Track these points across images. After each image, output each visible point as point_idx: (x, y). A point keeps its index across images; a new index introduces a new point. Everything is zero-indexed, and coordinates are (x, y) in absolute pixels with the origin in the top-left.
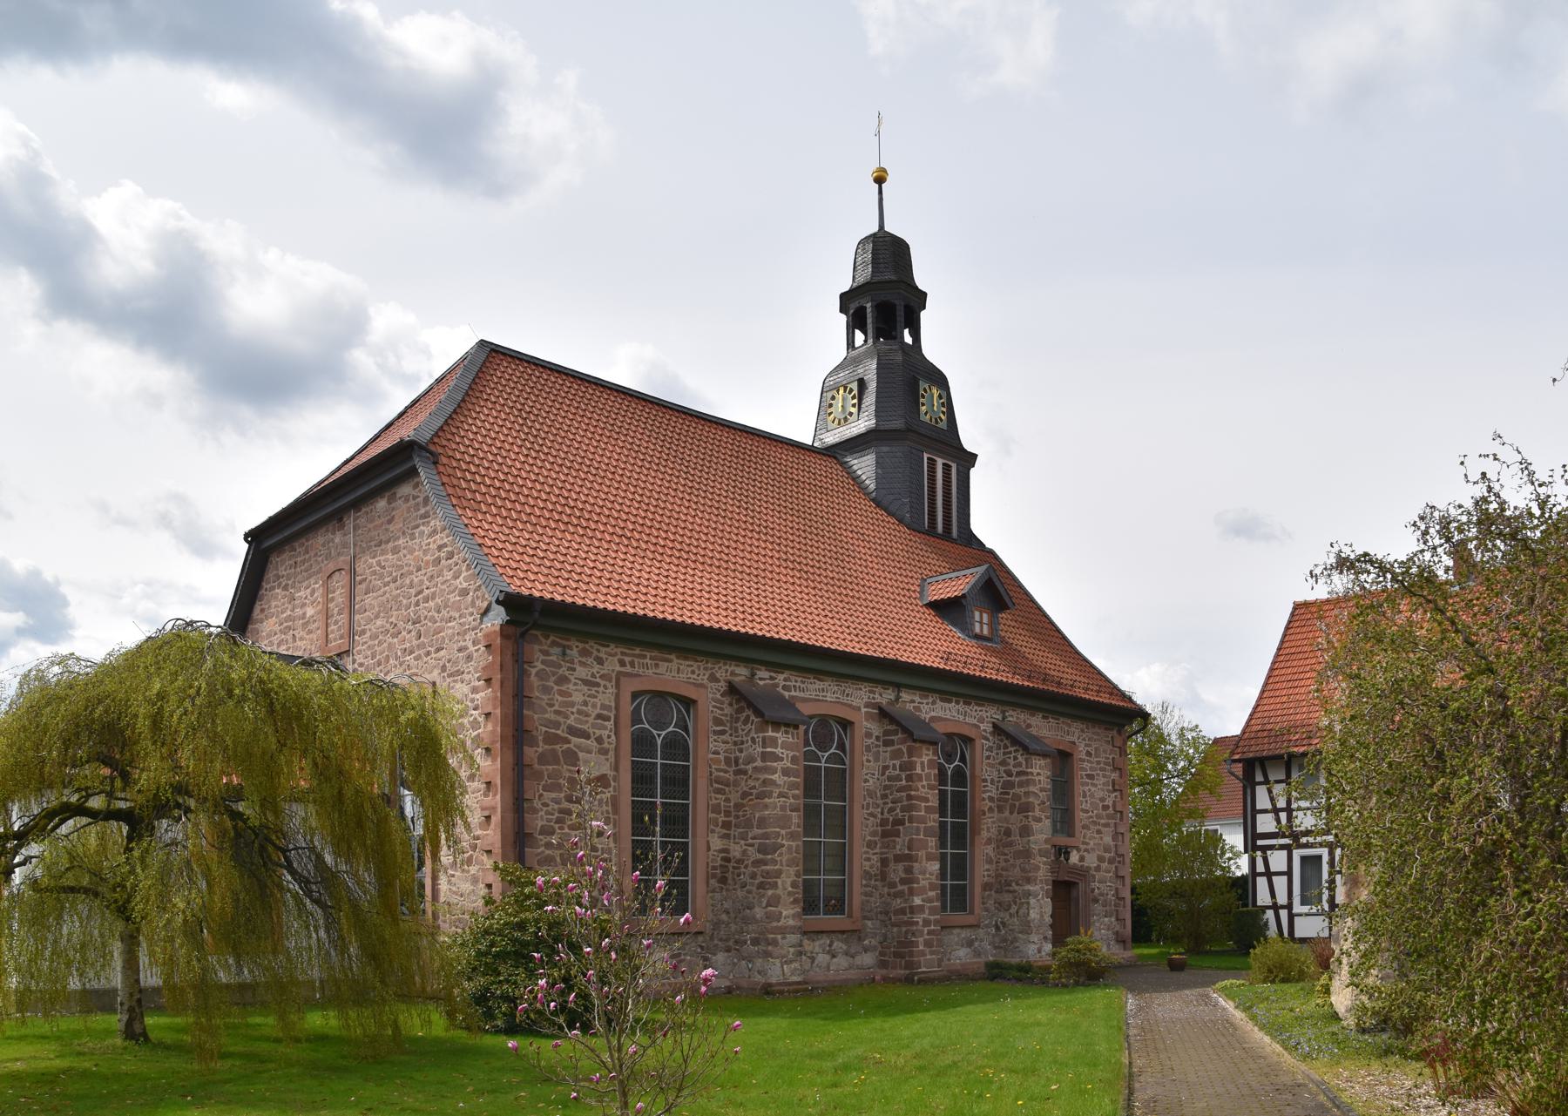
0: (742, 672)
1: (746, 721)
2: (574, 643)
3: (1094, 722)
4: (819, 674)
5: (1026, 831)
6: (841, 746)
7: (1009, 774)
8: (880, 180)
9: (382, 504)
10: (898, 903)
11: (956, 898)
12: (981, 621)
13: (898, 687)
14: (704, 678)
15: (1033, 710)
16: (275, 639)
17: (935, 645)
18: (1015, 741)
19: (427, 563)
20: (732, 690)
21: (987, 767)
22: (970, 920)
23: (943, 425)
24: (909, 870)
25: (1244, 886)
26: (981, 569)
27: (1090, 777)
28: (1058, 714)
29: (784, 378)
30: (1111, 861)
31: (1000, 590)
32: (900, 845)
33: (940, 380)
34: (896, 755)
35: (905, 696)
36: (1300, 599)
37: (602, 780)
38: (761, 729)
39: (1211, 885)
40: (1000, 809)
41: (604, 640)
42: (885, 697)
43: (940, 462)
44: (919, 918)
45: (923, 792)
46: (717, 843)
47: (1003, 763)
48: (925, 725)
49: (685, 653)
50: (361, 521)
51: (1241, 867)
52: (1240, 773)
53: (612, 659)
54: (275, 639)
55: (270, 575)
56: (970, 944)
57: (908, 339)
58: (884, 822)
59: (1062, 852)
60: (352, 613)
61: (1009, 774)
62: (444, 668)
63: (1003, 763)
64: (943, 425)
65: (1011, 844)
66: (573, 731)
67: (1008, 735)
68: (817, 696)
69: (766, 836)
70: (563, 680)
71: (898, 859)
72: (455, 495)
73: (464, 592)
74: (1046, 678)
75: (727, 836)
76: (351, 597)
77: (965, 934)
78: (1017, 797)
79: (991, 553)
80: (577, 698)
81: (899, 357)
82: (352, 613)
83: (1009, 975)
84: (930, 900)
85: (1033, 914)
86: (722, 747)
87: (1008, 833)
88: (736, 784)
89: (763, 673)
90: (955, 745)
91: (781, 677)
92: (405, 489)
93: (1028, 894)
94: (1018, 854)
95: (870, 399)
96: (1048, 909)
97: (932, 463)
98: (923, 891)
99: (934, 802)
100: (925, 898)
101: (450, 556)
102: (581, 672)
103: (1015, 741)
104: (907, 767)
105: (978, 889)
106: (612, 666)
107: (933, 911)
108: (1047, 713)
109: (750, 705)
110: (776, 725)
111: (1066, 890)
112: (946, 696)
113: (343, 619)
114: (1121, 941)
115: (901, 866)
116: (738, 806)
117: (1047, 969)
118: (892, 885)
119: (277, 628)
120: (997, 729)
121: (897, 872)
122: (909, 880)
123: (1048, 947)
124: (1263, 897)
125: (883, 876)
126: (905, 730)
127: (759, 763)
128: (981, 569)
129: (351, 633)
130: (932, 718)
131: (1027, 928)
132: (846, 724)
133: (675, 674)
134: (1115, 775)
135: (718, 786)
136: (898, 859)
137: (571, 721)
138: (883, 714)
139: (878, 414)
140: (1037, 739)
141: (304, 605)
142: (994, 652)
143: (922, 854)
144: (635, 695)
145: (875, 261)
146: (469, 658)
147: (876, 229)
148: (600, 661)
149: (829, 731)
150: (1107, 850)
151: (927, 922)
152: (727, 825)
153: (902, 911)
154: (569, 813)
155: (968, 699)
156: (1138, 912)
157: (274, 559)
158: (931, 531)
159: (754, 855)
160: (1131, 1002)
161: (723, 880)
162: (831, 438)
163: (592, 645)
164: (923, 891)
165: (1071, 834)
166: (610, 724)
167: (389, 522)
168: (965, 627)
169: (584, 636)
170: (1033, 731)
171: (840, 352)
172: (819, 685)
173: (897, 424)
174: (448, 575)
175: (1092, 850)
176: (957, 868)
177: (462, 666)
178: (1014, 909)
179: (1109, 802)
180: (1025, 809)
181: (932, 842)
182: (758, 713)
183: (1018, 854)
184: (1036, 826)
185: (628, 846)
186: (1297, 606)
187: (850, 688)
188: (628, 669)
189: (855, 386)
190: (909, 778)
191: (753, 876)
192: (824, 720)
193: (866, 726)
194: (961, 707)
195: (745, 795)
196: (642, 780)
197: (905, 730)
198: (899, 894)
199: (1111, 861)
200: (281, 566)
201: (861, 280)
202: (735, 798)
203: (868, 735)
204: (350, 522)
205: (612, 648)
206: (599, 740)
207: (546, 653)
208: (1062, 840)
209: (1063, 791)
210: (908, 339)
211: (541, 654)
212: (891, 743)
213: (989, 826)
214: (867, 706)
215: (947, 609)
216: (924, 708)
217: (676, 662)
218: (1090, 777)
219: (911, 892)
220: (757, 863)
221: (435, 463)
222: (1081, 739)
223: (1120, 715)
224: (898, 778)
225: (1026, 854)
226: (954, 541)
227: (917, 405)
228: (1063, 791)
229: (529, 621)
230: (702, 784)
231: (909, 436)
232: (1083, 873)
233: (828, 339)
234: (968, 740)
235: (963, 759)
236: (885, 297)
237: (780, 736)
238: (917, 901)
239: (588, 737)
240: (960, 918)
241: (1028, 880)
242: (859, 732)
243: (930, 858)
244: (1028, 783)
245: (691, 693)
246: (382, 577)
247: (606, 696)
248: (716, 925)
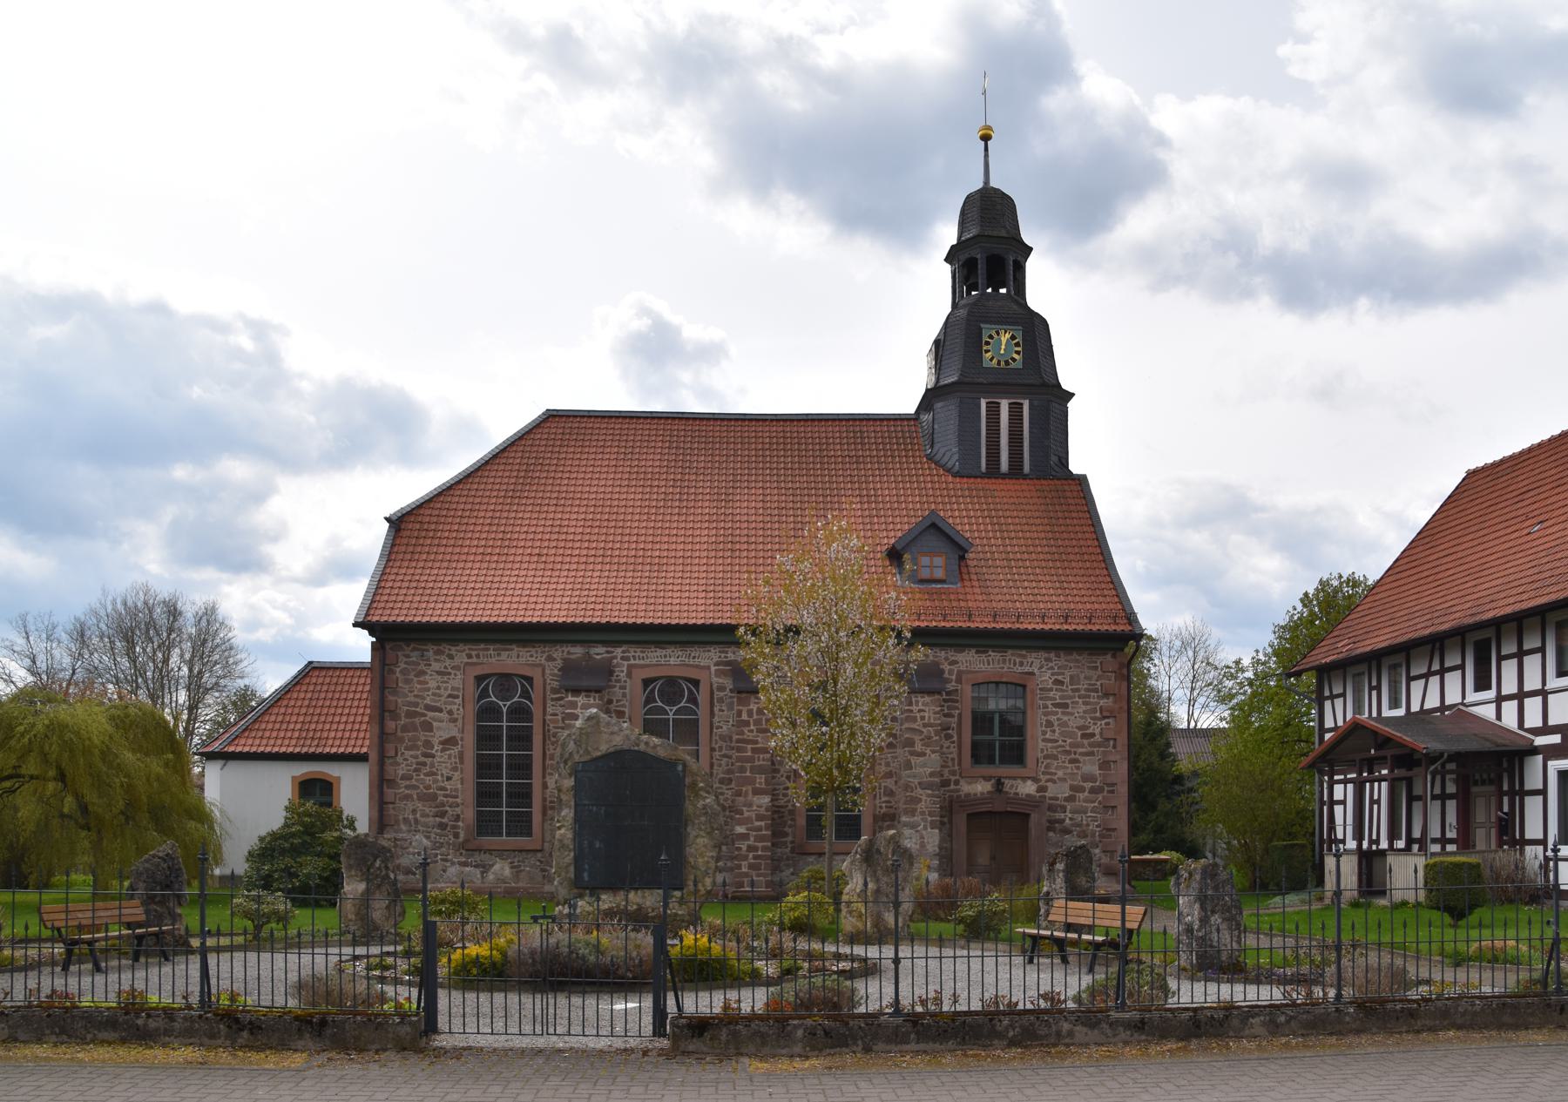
8: (986, 138)
37: (451, 741)
41: (454, 642)
43: (1004, 406)
49: (523, 643)
53: (461, 654)
66: (429, 708)
70: (423, 673)
80: (432, 684)
84: (760, 829)
91: (619, 650)
97: (994, 410)
102: (436, 666)
133: (514, 659)
137: (428, 701)
147: (980, 185)
148: (451, 657)
154: (424, 764)
158: (993, 471)
163: (445, 647)
172: (660, 652)
188: (474, 660)
196: (487, 738)
205: (461, 647)
206: (450, 712)
207: (408, 656)
211: (406, 658)
214: (717, 664)
217: (516, 649)
233: (927, 294)
239: (441, 711)
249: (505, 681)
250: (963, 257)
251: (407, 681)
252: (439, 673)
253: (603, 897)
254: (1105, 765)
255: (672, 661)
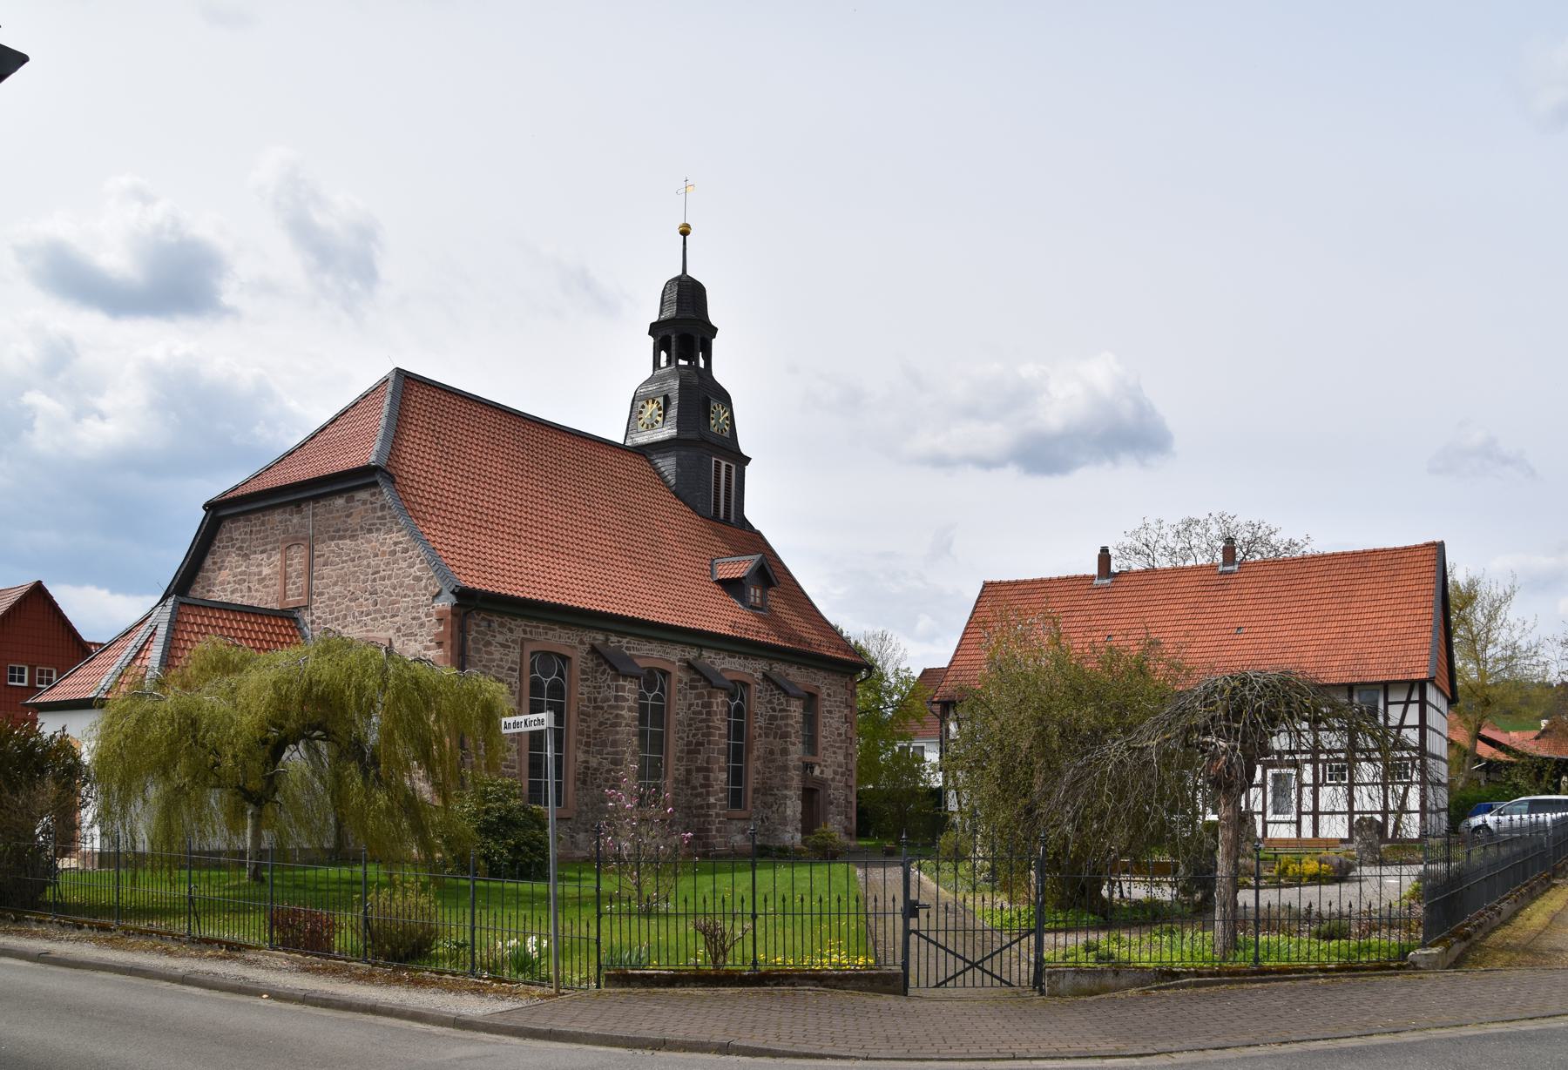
0: (600, 637)
1: (603, 673)
2: (495, 618)
3: (833, 672)
4: (649, 639)
5: (785, 752)
6: (662, 689)
7: (774, 710)
8: (685, 232)
9: (340, 502)
10: (698, 801)
11: (736, 799)
12: (754, 594)
13: (701, 647)
14: (576, 642)
15: (791, 663)
16: (229, 588)
17: (723, 617)
18: (779, 687)
19: (384, 553)
20: (594, 650)
21: (759, 704)
22: (744, 814)
23: (726, 434)
24: (707, 778)
25: (937, 795)
26: (757, 557)
27: (830, 712)
28: (808, 666)
29: (599, 387)
30: (843, 774)
31: (770, 575)
32: (700, 760)
33: (725, 398)
34: (700, 696)
35: (705, 654)
36: (989, 579)
38: (615, 679)
39: (913, 794)
40: (767, 736)
41: (514, 616)
42: (691, 654)
43: (724, 464)
44: (713, 812)
45: (717, 723)
46: (581, 757)
47: (770, 702)
48: (718, 675)
49: (564, 625)
50: (320, 510)
51: (937, 781)
52: (938, 711)
54: (229, 588)
55: (223, 535)
56: (744, 831)
57: (702, 364)
58: (689, 744)
59: (808, 767)
60: (310, 578)
61: (774, 710)
62: (399, 630)
63: (770, 702)
64: (726, 434)
65: (774, 761)
67: (774, 683)
68: (648, 654)
69: (616, 753)
70: (488, 644)
71: (699, 770)
72: (410, 509)
73: (418, 579)
74: (801, 640)
75: (587, 752)
76: (310, 566)
77: (741, 824)
78: (779, 727)
79: (759, 533)
80: (497, 656)
81: (696, 381)
82: (310, 578)
83: (766, 853)
85: (789, 812)
86: (586, 690)
87: (772, 752)
88: (595, 715)
89: (613, 638)
90: (737, 689)
92: (363, 495)
93: (786, 797)
94: (779, 768)
95: (673, 412)
96: (799, 809)
97: (718, 465)
98: (716, 793)
99: (724, 731)
100: (717, 798)
101: (406, 551)
102: (500, 638)
103: (779, 687)
104: (708, 705)
105: (750, 793)
106: (518, 634)
107: (722, 808)
108: (800, 665)
109: (607, 661)
110: (625, 677)
111: (811, 794)
112: (732, 653)
113: (302, 582)
114: (848, 833)
115: (701, 775)
116: (596, 732)
117: (799, 851)
118: (694, 788)
119: (231, 579)
120: (766, 677)
121: (698, 779)
122: (707, 785)
123: (799, 836)
124: (953, 806)
125: (687, 782)
126: (706, 679)
127: (612, 702)
128: (757, 557)
129: (310, 593)
130: (723, 670)
131: (784, 821)
132: (665, 673)
133: (558, 639)
134: (846, 711)
135: (584, 716)
136: (699, 770)
138: (690, 666)
139: (680, 425)
140: (791, 684)
141: (260, 565)
142: (762, 619)
143: (716, 767)
144: (533, 654)
145: (679, 301)
146: (422, 625)
148: (511, 630)
149: (653, 679)
150: (840, 766)
151: (718, 815)
152: (588, 744)
153: (701, 807)
155: (746, 656)
156: (861, 812)
157: (227, 525)
158: (716, 518)
159: (607, 765)
160: (859, 872)
161: (584, 782)
162: (642, 439)
163: (506, 620)
164: (716, 793)
165: (815, 754)
166: (516, 674)
167: (348, 516)
168: (742, 598)
169: (501, 614)
170: (790, 678)
171: (648, 371)
172: (649, 646)
173: (692, 435)
174: (404, 565)
175: (829, 766)
176: (737, 776)
177: (415, 630)
178: (775, 807)
179: (842, 731)
180: (785, 736)
181: (723, 759)
182: (612, 667)
183: (779, 768)
184: (792, 748)
185: (526, 758)
186: (986, 585)
187: (668, 648)
189: (661, 400)
190: (708, 713)
191: (607, 780)
192: (651, 671)
193: (678, 674)
194: (742, 661)
195: (601, 724)
197: (706, 679)
198: (700, 795)
199: (843, 774)
200: (235, 531)
201: (667, 315)
202: (594, 725)
203: (680, 681)
204: (308, 509)
205: (519, 622)
206: (510, 684)
208: (809, 759)
209: (810, 720)
210: (702, 364)
211: (476, 625)
212: (695, 688)
213: (758, 747)
215: (732, 586)
216: (718, 662)
217: (558, 630)
218: (830, 712)
219: (708, 794)
220: (609, 771)
221: (394, 482)
222: (823, 684)
223: (851, 664)
224: (700, 713)
225: (785, 768)
226: (732, 525)
227: (708, 419)
228: (810, 720)
229: (473, 608)
230: (573, 715)
231: (696, 442)
232: (823, 783)
233: (637, 360)
234: (745, 685)
235: (742, 699)
236: (684, 326)
237: (628, 685)
238: (712, 800)
240: (737, 813)
241: (786, 787)
242: (674, 679)
243: (721, 770)
244: (787, 717)
245: (566, 652)
246: (339, 555)
247: (514, 655)
248: (580, 813)
249: (546, 656)
250: (661, 334)
251: (478, 651)
252: (502, 645)
253: (236, 535)
254: (847, 755)
255: (656, 655)
